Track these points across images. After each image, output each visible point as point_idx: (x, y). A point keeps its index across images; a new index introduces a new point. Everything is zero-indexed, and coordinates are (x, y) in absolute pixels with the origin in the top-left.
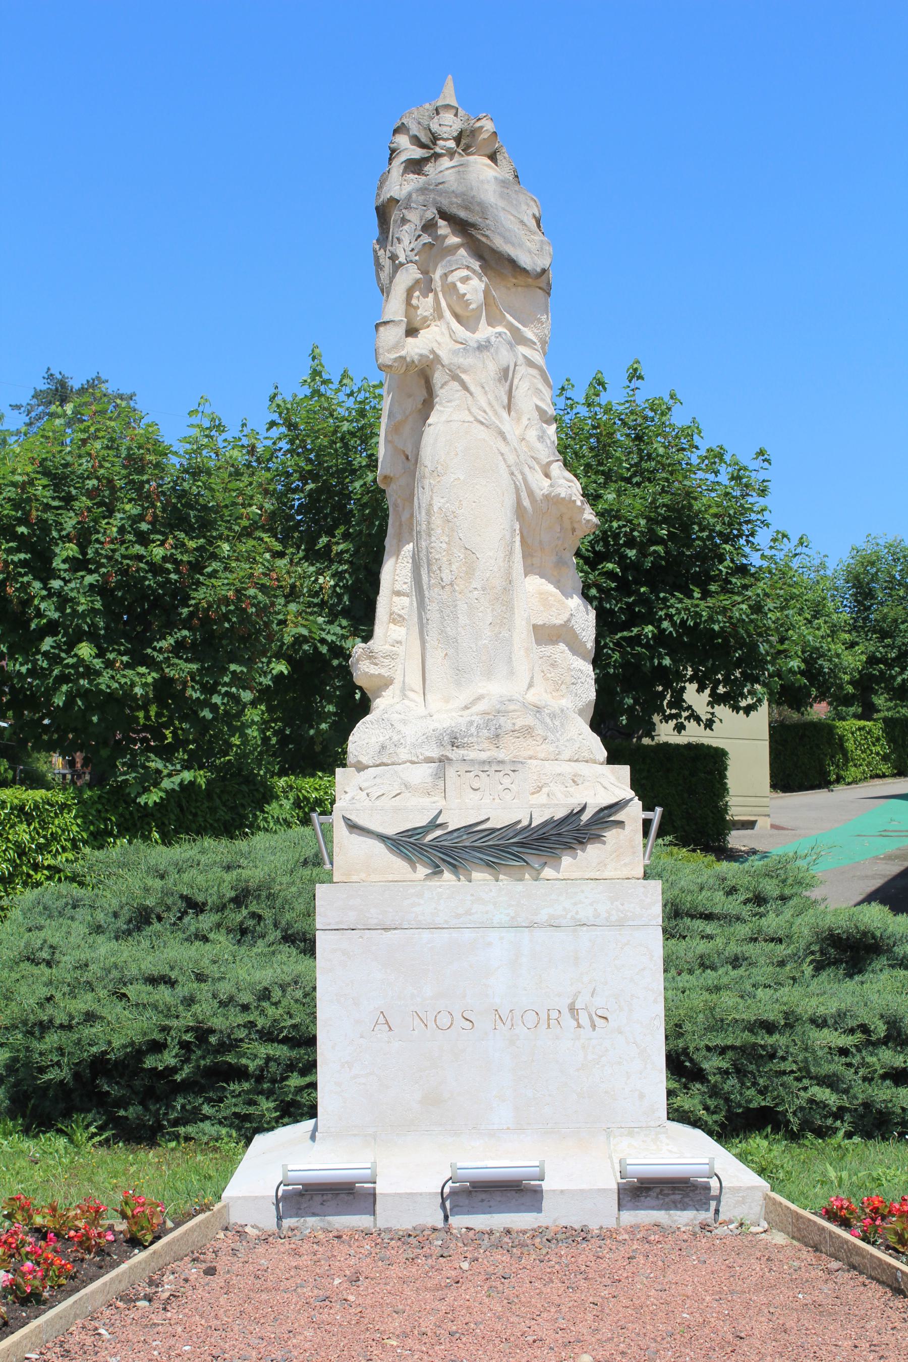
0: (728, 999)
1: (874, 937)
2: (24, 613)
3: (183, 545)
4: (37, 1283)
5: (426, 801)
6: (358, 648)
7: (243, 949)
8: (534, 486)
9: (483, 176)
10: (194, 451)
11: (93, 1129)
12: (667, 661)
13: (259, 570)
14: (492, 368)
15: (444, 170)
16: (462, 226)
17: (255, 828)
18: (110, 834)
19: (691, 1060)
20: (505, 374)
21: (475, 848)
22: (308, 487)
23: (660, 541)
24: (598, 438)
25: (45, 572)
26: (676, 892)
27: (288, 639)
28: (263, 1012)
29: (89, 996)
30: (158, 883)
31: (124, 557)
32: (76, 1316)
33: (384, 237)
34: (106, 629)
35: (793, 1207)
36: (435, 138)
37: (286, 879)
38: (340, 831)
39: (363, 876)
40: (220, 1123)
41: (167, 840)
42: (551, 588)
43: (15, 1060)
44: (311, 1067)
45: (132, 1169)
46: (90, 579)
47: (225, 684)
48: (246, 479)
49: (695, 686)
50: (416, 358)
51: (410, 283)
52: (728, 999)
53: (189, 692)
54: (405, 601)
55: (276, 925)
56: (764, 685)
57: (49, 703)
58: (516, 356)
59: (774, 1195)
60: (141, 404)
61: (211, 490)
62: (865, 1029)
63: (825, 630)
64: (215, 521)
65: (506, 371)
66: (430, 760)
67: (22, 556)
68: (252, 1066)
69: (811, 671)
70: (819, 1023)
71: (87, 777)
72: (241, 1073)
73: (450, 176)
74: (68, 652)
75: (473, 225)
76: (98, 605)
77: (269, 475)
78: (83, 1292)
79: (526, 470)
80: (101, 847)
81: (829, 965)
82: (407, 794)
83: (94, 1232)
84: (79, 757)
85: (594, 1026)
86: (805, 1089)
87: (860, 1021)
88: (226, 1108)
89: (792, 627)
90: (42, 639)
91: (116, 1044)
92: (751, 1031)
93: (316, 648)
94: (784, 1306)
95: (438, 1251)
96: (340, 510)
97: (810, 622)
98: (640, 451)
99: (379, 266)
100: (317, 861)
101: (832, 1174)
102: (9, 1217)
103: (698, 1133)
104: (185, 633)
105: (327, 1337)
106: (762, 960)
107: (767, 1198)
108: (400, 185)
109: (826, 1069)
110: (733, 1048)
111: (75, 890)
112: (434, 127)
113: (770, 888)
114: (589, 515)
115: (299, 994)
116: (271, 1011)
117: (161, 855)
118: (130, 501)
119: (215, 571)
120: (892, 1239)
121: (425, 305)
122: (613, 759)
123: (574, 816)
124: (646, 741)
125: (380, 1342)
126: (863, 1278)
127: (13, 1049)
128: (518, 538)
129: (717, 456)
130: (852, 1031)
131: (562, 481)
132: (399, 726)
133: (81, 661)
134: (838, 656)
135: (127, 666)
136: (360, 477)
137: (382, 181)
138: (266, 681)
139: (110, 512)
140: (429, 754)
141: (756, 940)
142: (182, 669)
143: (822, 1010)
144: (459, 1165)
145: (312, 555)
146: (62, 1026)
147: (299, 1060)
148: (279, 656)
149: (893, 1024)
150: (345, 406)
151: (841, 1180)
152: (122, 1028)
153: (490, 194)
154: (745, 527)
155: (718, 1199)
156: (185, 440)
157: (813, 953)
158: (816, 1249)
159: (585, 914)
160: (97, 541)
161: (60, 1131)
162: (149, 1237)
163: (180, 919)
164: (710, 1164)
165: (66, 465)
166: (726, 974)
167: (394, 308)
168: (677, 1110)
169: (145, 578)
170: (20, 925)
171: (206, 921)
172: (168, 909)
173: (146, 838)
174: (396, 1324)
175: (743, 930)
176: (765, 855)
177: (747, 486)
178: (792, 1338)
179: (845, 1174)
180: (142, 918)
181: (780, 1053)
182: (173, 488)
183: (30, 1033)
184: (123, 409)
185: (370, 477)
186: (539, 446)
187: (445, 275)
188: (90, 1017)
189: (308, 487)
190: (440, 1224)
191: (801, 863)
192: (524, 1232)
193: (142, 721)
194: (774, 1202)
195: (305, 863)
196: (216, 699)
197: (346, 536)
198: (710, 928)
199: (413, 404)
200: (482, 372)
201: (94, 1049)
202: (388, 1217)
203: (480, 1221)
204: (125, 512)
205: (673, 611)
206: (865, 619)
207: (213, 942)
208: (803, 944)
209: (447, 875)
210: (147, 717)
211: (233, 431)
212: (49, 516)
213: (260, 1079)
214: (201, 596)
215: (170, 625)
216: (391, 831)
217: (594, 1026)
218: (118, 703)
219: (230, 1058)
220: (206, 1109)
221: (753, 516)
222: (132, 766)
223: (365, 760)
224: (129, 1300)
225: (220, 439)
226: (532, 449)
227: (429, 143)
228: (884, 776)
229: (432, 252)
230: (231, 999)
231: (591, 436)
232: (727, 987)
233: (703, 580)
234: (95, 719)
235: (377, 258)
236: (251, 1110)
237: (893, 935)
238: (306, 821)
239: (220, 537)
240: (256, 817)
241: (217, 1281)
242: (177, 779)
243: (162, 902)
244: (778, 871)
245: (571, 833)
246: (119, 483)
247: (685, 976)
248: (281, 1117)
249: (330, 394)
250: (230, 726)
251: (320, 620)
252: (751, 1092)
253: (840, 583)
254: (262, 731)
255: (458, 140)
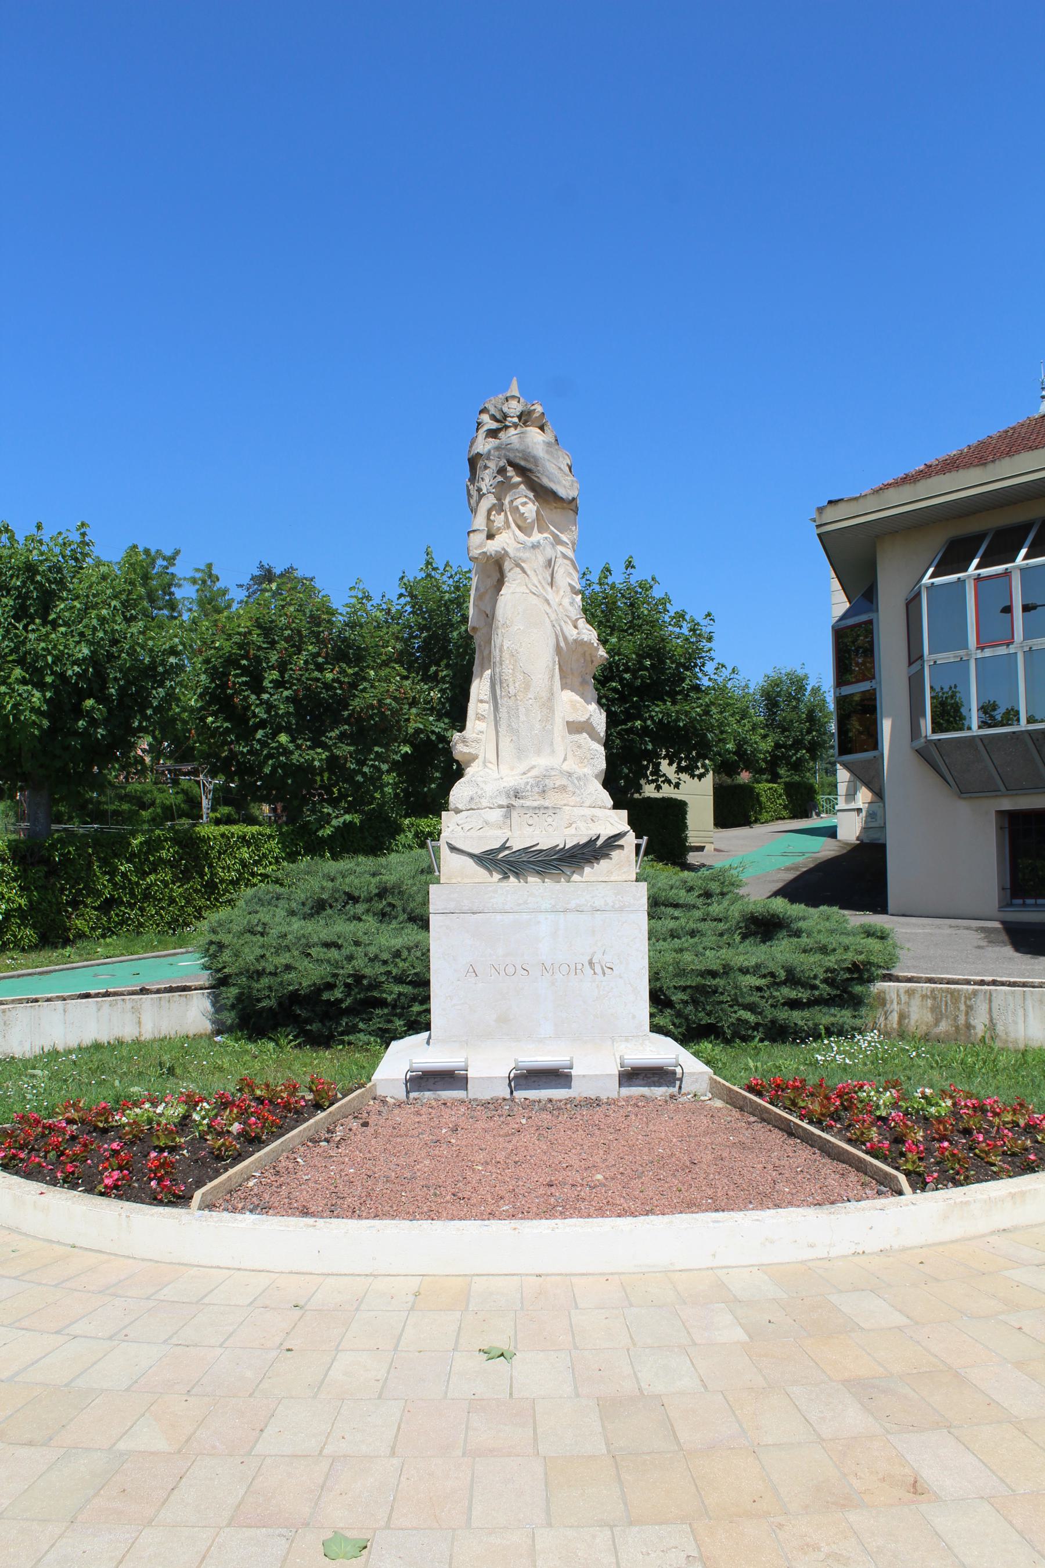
0: (688, 957)
1: (778, 917)
2: (245, 715)
3: (345, 671)
4: (258, 1130)
5: (499, 832)
6: (457, 736)
7: (383, 926)
8: (567, 634)
9: (536, 439)
10: (353, 613)
11: (291, 1037)
12: (650, 747)
13: (393, 687)
14: (541, 560)
15: (511, 436)
16: (521, 471)
17: (390, 850)
18: (299, 854)
19: (665, 995)
20: (549, 563)
21: (529, 862)
22: (423, 635)
23: (646, 669)
24: (606, 604)
25: (259, 690)
26: (655, 890)
27: (411, 731)
28: (396, 965)
29: (288, 955)
30: (330, 884)
31: (308, 679)
32: (283, 1151)
33: (473, 478)
34: (296, 724)
35: (727, 1084)
36: (505, 416)
37: (410, 882)
38: (445, 851)
39: (459, 879)
40: (370, 1034)
41: (335, 857)
42: (578, 698)
43: (241, 994)
44: (427, 999)
45: (315, 1062)
46: (286, 693)
47: (371, 760)
48: (385, 630)
49: (667, 761)
50: (493, 553)
51: (489, 506)
52: (688, 957)
53: (348, 764)
54: (486, 706)
55: (404, 911)
56: (710, 760)
57: (260, 771)
58: (556, 551)
59: (715, 1077)
60: (318, 584)
61: (364, 637)
62: (772, 975)
63: (748, 727)
64: (365, 656)
65: (550, 561)
66: (501, 807)
67: (244, 679)
68: (389, 999)
69: (740, 752)
70: (744, 971)
71: (284, 819)
72: (382, 1003)
73: (515, 440)
74: (273, 739)
75: (530, 471)
76: (291, 710)
77: (399, 628)
78: (287, 1136)
79: (563, 623)
80: (294, 862)
81: (750, 935)
82: (486, 828)
83: (293, 1100)
84: (279, 806)
85: (604, 974)
86: (735, 1012)
87: (770, 970)
88: (374, 1024)
89: (728, 725)
90: (256, 732)
91: (304, 984)
92: (702, 976)
93: (428, 737)
94: (720, 1144)
95: (506, 1113)
96: (444, 647)
97: (739, 722)
98: (633, 613)
99: (470, 495)
100: (430, 870)
101: (751, 1064)
102: (240, 1090)
103: (669, 1039)
104: (346, 727)
105: (438, 1164)
106: (709, 933)
107: (711, 1079)
108: (483, 445)
109: (749, 999)
110: (690, 987)
111: (278, 888)
112: (505, 409)
113: (714, 887)
114: (602, 652)
115: (419, 954)
116: (401, 964)
117: (332, 866)
118: (312, 644)
119: (365, 688)
120: (788, 1103)
121: (499, 520)
122: (616, 806)
123: (592, 842)
124: (637, 796)
125: (471, 1168)
126: (770, 1127)
127: (240, 987)
128: (557, 667)
129: (681, 616)
130: (764, 976)
131: (585, 631)
132: (482, 785)
133: (281, 745)
134: (756, 743)
135: (309, 748)
136: (457, 629)
137: (473, 442)
138: (397, 758)
139: (299, 651)
140: (501, 803)
141: (705, 920)
142: (345, 750)
143: (746, 964)
144: (520, 1059)
145: (426, 679)
146: (270, 973)
147: (419, 995)
148: (405, 742)
149: (790, 971)
150: (447, 584)
151: (756, 1067)
152: (308, 974)
153: (540, 451)
154: (698, 661)
155: (681, 1080)
156: (347, 605)
157: (740, 928)
158: (741, 1109)
159: (599, 903)
160: (291, 669)
161: (270, 1039)
162: (327, 1104)
163: (344, 907)
164: (677, 1059)
165: (272, 622)
166: (687, 941)
167: (480, 522)
168: (655, 1026)
169: (321, 693)
170: (244, 910)
171: (360, 908)
172: (336, 900)
173: (322, 856)
174: (481, 1156)
175: (698, 914)
176: (710, 867)
177: (699, 635)
178: (726, 1163)
179: (759, 1064)
180: (320, 906)
181: (720, 990)
182: (339, 636)
183: (250, 977)
184: (307, 587)
185: (463, 628)
186: (571, 608)
187: (512, 501)
188: (288, 968)
189: (423, 635)
190: (508, 1096)
191: (733, 872)
192: (560, 1101)
193: (319, 783)
194: (716, 1081)
195: (422, 872)
196: (366, 769)
197: (447, 666)
198: (677, 913)
199: (491, 582)
200: (535, 562)
201: (291, 988)
202: (475, 1091)
203: (533, 1094)
204: (308, 651)
205: (653, 714)
206: (774, 719)
207: (364, 921)
208: (734, 922)
209: (512, 879)
210: (322, 780)
211: (376, 600)
212: (261, 653)
213: (394, 1007)
214: (356, 703)
215: (337, 722)
216: (477, 851)
217: (604, 974)
218: (306, 771)
219: (376, 994)
220: (361, 1025)
221: (704, 654)
222: (313, 811)
223: (460, 807)
224: (315, 1141)
225: (369, 604)
226: (566, 610)
227: (501, 419)
228: (784, 818)
229: (503, 488)
230: (376, 957)
231: (602, 603)
232: (687, 949)
233: (673, 695)
234: (290, 781)
235: (468, 491)
236: (389, 1026)
237: (790, 916)
238: (423, 845)
239: (368, 667)
240: (391, 843)
241: (369, 1131)
242: (341, 820)
243: (332, 896)
244: (720, 877)
245: (590, 852)
246: (304, 633)
247: (661, 943)
248: (408, 1030)
249: (438, 576)
250: (374, 785)
251: (431, 718)
252: (701, 1015)
253: (758, 697)
254: (394, 789)
255: (520, 417)
